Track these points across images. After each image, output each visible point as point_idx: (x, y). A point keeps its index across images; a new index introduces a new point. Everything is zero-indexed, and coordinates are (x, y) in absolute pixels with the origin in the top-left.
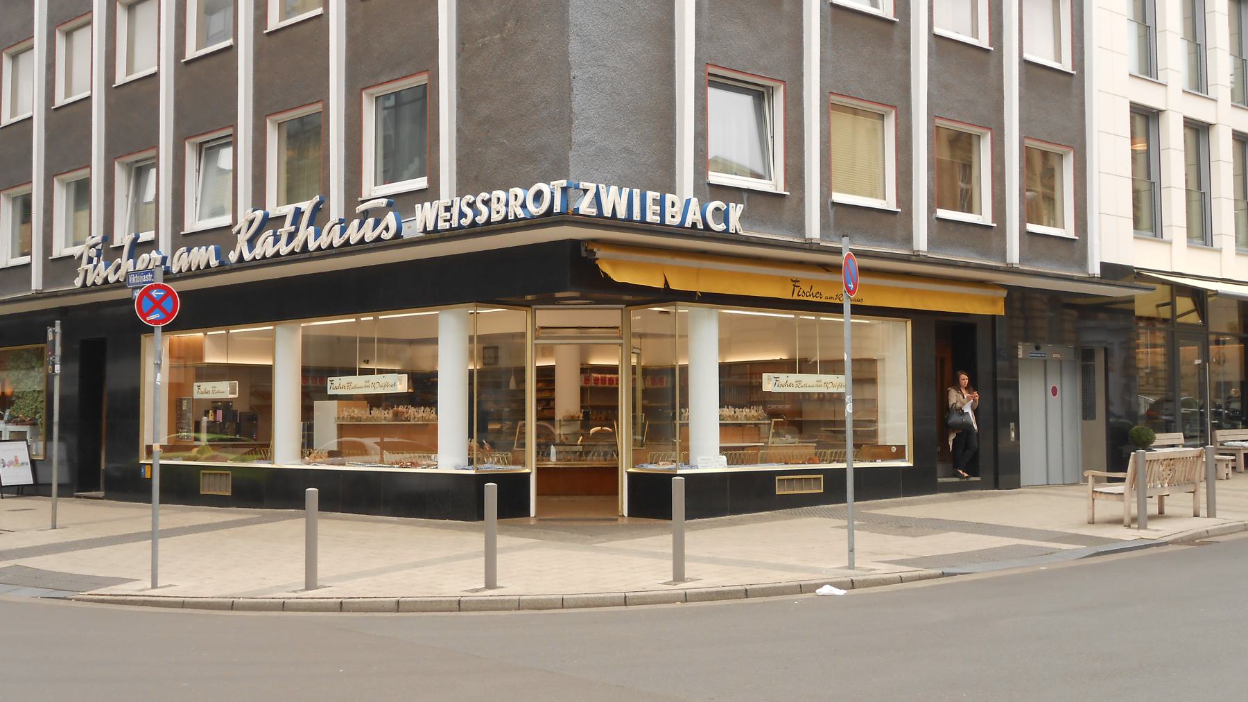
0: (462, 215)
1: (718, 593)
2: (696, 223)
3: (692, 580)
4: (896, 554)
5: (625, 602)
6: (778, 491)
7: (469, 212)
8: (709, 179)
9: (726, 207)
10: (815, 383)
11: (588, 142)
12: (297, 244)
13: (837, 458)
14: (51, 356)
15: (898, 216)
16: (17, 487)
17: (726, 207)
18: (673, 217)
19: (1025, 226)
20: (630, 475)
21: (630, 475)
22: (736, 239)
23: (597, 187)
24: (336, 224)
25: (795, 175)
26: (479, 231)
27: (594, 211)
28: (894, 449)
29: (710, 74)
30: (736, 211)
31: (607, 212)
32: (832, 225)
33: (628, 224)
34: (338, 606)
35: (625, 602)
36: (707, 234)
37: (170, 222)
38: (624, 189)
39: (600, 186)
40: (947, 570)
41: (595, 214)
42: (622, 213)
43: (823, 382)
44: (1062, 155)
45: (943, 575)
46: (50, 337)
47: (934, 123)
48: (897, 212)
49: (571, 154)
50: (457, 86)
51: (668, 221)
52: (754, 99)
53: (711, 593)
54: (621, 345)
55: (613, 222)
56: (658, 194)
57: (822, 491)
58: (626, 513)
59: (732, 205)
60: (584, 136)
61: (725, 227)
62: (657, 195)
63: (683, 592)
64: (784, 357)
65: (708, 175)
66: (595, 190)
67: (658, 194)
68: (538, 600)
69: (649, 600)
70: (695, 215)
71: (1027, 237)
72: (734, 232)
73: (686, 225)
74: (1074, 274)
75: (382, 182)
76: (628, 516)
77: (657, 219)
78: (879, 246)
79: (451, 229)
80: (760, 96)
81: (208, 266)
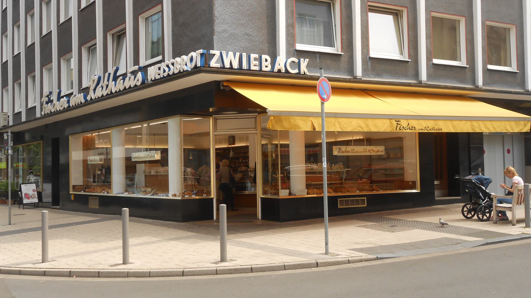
0: (164, 71)
1: (235, 269)
2: (280, 69)
3: (232, 260)
4: (369, 243)
5: (183, 274)
6: (340, 206)
7: (167, 69)
8: (370, 55)
9: (298, 61)
10: (363, 150)
11: (224, 31)
12: (108, 91)
13: (387, 188)
14: (6, 146)
15: (409, 63)
16: (34, 204)
17: (298, 61)
18: (266, 67)
19: (487, 66)
20: (262, 198)
21: (262, 198)
22: (305, 77)
23: (221, 54)
24: (122, 79)
25: (349, 45)
26: (164, 80)
27: (218, 65)
28: (411, 183)
29: (369, 6)
30: (304, 63)
31: (227, 65)
32: (370, 69)
33: (240, 71)
34: (43, 273)
35: (183, 274)
36: (287, 75)
37: (77, 84)
38: (237, 53)
39: (223, 52)
40: (379, 256)
41: (258, 70)
42: (236, 65)
43: (367, 150)
44: (510, 29)
45: (377, 259)
46: (6, 138)
47: (431, 14)
48: (409, 61)
49: (215, 37)
50: (172, 8)
51: (264, 69)
52: (394, 18)
53: (231, 270)
54: (257, 133)
55: (231, 70)
56: (257, 55)
57: (366, 206)
58: (260, 218)
59: (302, 60)
60: (222, 28)
61: (298, 71)
62: (257, 56)
63: (215, 268)
64: (361, 138)
65: (296, 45)
66: (219, 54)
67: (257, 55)
68: (137, 272)
69: (196, 273)
70: (279, 65)
71: (488, 72)
72: (303, 73)
73: (275, 71)
74: (512, 90)
75: (150, 58)
76: (262, 219)
77: (257, 68)
78: (398, 79)
79: (161, 78)
80: (396, 15)
81: (81, 103)
